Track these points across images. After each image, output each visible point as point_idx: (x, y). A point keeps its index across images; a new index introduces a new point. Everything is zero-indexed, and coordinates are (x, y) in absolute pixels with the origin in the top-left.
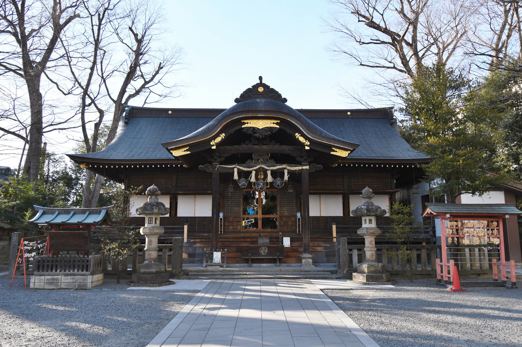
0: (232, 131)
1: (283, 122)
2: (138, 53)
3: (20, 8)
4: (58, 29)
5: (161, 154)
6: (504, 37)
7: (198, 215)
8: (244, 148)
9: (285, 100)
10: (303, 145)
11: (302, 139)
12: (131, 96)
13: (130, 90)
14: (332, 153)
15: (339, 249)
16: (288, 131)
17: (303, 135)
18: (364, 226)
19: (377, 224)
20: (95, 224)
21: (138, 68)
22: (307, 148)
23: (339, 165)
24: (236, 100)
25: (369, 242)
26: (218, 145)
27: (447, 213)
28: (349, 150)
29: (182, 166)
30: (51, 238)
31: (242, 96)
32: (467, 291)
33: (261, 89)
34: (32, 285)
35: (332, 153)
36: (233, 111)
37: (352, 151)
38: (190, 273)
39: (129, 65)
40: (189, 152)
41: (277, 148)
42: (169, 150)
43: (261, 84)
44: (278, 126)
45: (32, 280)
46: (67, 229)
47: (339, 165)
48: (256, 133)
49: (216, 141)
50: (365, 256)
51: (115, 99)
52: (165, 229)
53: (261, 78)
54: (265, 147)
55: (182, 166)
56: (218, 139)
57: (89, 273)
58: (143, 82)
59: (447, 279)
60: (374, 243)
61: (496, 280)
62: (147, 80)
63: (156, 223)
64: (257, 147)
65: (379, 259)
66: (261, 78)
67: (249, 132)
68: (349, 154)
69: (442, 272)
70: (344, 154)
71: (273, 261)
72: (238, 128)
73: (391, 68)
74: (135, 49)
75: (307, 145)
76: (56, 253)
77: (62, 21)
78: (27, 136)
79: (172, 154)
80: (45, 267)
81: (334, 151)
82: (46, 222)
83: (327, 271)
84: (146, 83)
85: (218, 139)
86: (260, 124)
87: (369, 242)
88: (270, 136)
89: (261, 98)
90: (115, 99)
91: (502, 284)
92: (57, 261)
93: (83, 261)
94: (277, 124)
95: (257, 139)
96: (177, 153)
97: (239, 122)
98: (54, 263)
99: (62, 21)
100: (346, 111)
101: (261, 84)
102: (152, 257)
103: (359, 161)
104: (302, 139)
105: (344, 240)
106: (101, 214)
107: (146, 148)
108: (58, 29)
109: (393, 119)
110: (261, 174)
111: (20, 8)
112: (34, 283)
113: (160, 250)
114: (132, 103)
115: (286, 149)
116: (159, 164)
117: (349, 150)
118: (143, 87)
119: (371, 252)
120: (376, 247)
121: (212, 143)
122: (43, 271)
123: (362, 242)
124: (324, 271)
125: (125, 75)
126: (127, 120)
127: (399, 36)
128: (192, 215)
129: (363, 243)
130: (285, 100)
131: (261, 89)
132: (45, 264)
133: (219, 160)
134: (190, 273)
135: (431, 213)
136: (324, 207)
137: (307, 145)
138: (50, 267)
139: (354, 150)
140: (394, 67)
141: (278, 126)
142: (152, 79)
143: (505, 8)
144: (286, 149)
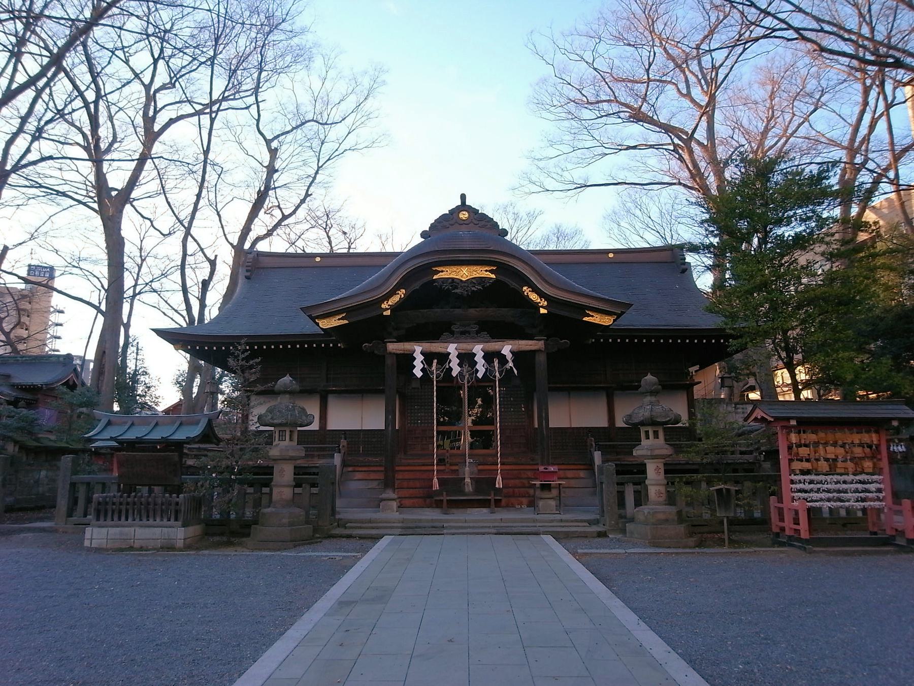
0: (417, 285)
1: (501, 268)
2: (271, 170)
3: (93, 110)
4: (151, 137)
5: (302, 326)
6: (863, 130)
7: (366, 427)
8: (437, 313)
9: (505, 233)
10: (536, 307)
11: (534, 297)
12: (259, 239)
13: (258, 229)
14: (586, 319)
15: (602, 483)
16: (513, 284)
17: (535, 290)
18: (644, 442)
19: (666, 440)
20: (189, 441)
21: (271, 192)
22: (543, 311)
23: (598, 340)
24: (424, 234)
25: (654, 473)
26: (393, 309)
27: (793, 418)
28: (614, 314)
29: (335, 345)
30: (120, 465)
31: (433, 226)
32: (749, 544)
33: (464, 215)
34: (87, 543)
35: (586, 319)
36: (415, 253)
37: (619, 316)
38: (348, 525)
39: (257, 189)
40: (346, 322)
41: (492, 312)
42: (313, 319)
43: (463, 206)
44: (493, 276)
45: (88, 535)
46: (143, 450)
47: (598, 340)
48: (456, 288)
49: (390, 303)
50: (647, 495)
51: (235, 244)
52: (307, 449)
53: (463, 197)
54: (472, 311)
55: (335, 345)
56: (395, 299)
57: (180, 523)
58: (280, 216)
59: (792, 534)
60: (662, 471)
61: (875, 533)
62: (286, 214)
63: (291, 440)
64: (458, 311)
65: (671, 500)
66: (463, 197)
67: (446, 287)
68: (614, 321)
69: (782, 519)
70: (607, 321)
71: (484, 504)
72: (425, 280)
73: (674, 184)
74: (266, 164)
75: (542, 307)
76: (130, 489)
77: (157, 128)
78: (100, 303)
79: (318, 324)
80: (151, 513)
81: (589, 316)
82: (112, 439)
83: (582, 521)
84: (285, 217)
85: (395, 299)
86: (464, 273)
87: (654, 473)
88: (481, 293)
89: (464, 231)
90: (235, 244)
91: (888, 541)
92: (121, 504)
93: (121, 504)
94: (491, 271)
95: (459, 297)
96: (326, 324)
97: (428, 269)
98: (123, 508)
99: (157, 128)
100: (607, 252)
101: (463, 206)
102: (283, 497)
103: (631, 333)
104: (534, 297)
105: (611, 466)
106: (200, 425)
107: (285, 320)
108: (151, 137)
109: (685, 263)
110: (469, 355)
111: (93, 110)
112: (92, 539)
113: (298, 485)
114: (262, 247)
115: (506, 314)
116: (298, 343)
117: (614, 314)
118: (278, 224)
119: (657, 488)
120: (665, 478)
121: (383, 306)
122: (162, 520)
123: (641, 469)
124: (577, 521)
125: (251, 205)
126: (248, 274)
127: (686, 133)
128: (358, 427)
129: (644, 472)
130: (505, 233)
131: (464, 215)
132: (109, 507)
133: (395, 333)
134: (348, 525)
135: (763, 418)
136: (571, 414)
137: (542, 307)
138: (124, 513)
139: (623, 313)
140: (680, 184)
141: (493, 276)
142: (294, 212)
143: (864, 84)
144: (506, 314)
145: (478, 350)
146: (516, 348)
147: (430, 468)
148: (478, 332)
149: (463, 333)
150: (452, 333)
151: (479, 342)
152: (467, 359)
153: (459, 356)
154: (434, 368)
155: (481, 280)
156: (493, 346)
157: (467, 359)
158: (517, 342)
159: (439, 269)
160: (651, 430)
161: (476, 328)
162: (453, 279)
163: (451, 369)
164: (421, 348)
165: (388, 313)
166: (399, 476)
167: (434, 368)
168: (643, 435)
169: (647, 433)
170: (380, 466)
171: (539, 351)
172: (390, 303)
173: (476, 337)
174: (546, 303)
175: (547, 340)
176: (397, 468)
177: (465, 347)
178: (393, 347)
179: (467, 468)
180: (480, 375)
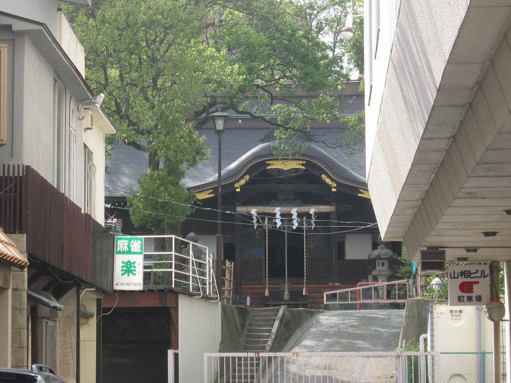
10: (330, 187)
14: (359, 195)
17: (329, 177)
18: (378, 268)
22: (334, 190)
44: (304, 168)
48: (281, 174)
49: (331, 183)
81: (361, 193)
85: (243, 182)
88: (296, 177)
94: (303, 165)
104: (328, 181)
137: (333, 187)
141: (304, 168)
145: (294, 211)
146: (318, 211)
147: (271, 286)
148: (294, 200)
149: (284, 200)
150: (277, 200)
151: (278, 206)
152: (287, 217)
153: (282, 215)
154: (266, 223)
155: (296, 170)
156: (304, 209)
157: (287, 217)
158: (318, 207)
159: (270, 162)
160: (381, 262)
161: (292, 197)
162: (279, 169)
163: (276, 223)
164: (255, 210)
165: (238, 190)
166: (11, 175)
167: (266, 223)
168: (377, 265)
169: (379, 263)
170: (244, 288)
171: (332, 212)
172: (240, 184)
173: (293, 203)
174: (335, 185)
175: (338, 205)
176: (243, 286)
177: (286, 210)
178: (241, 210)
179: (286, 286)
180: (294, 228)
